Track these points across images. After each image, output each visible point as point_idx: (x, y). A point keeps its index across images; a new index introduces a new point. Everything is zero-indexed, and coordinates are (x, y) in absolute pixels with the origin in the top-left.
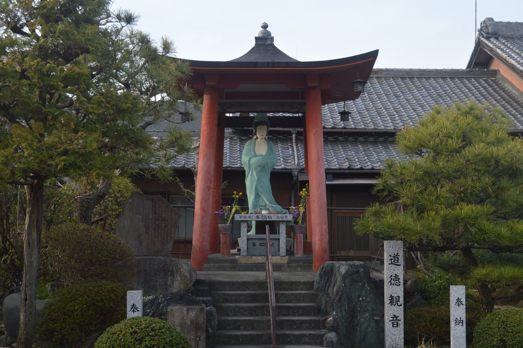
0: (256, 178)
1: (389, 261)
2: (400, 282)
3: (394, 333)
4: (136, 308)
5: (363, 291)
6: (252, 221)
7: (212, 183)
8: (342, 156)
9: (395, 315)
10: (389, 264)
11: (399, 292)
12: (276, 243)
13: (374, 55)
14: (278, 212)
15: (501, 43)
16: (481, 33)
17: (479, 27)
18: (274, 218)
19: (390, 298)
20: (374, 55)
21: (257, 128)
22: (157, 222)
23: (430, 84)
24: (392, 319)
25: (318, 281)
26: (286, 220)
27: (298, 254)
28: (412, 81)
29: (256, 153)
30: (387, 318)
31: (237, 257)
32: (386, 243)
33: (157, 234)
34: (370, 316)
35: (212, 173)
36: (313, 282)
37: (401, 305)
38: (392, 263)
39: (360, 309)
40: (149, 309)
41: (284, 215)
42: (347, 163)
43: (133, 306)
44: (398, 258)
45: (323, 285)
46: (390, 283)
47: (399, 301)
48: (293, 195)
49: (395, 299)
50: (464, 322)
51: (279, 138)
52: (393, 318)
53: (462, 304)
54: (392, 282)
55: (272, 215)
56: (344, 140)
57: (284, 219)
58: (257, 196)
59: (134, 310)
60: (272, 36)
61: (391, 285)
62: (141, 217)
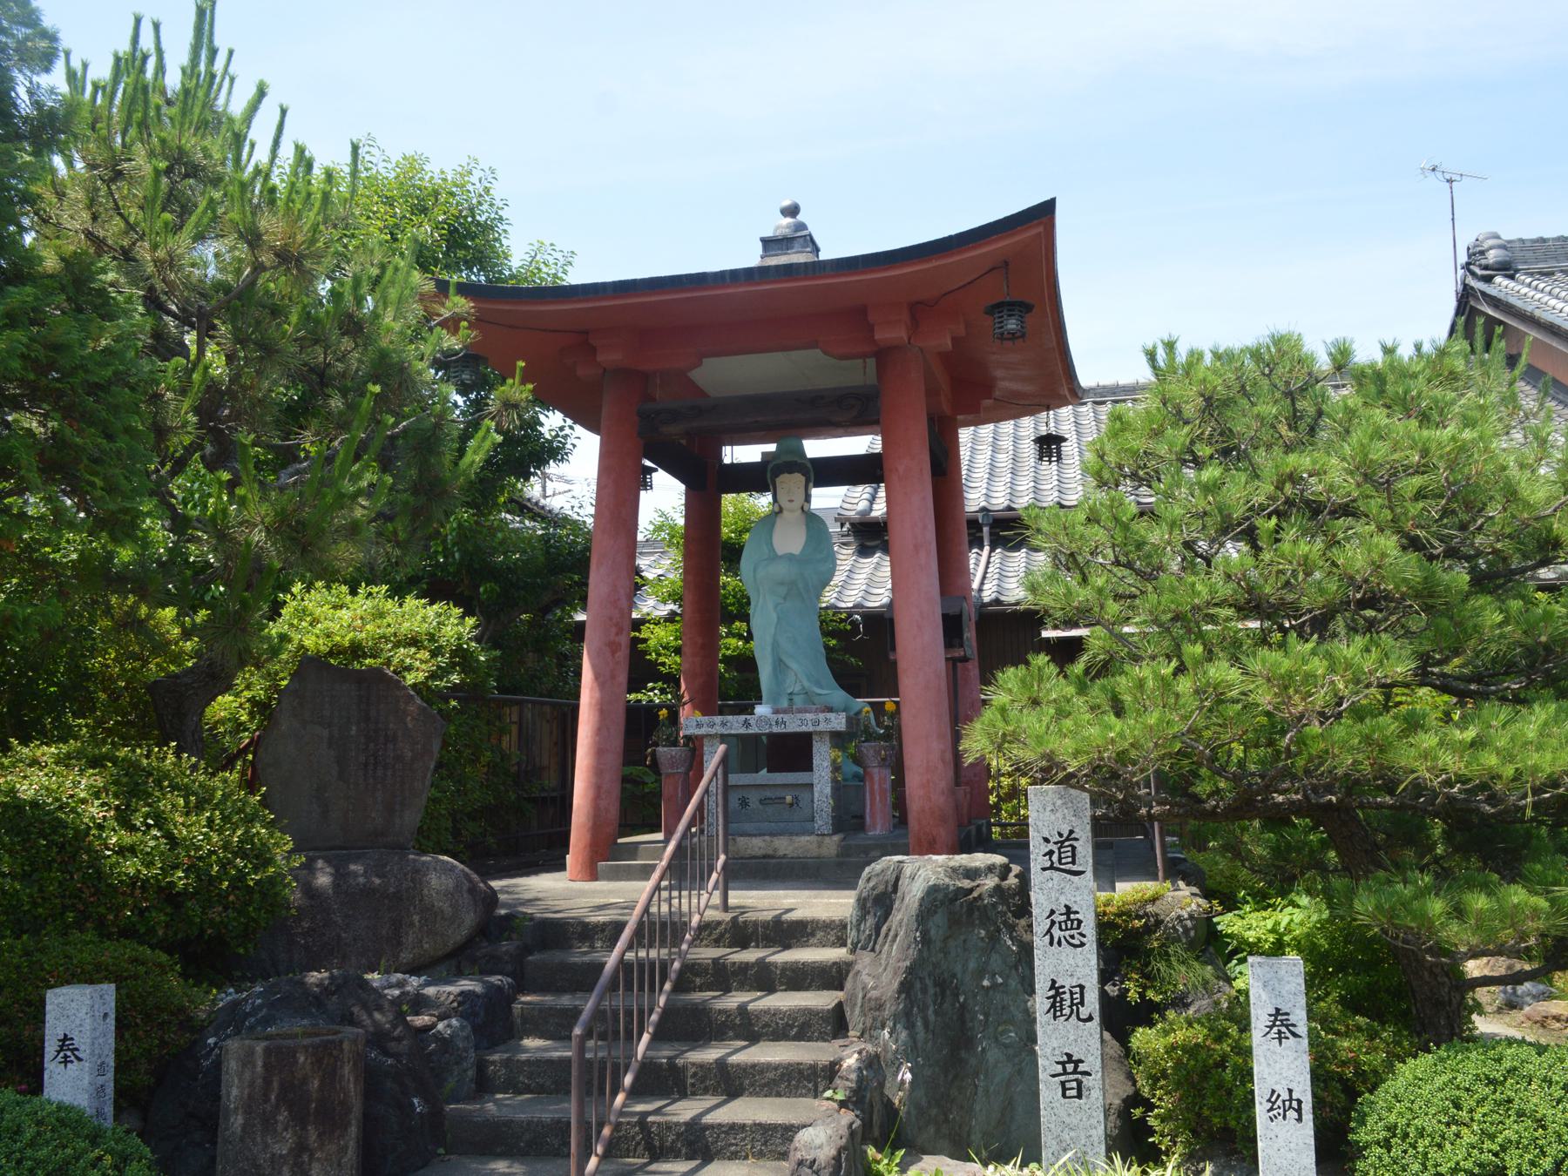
0: (774, 616)
2: (1084, 936)
3: (1068, 1120)
9: (1069, 1056)
10: (1044, 869)
11: (1080, 972)
12: (804, 796)
13: (1045, 211)
16: (1469, 271)
17: (1463, 258)
19: (1052, 993)
21: (778, 480)
24: (1059, 1068)
25: (854, 921)
26: (829, 727)
29: (775, 546)
30: (1047, 1064)
33: (371, 781)
34: (1021, 1039)
37: (1090, 1019)
38: (1052, 867)
39: (986, 1015)
40: (214, 1036)
44: (1074, 848)
46: (1048, 937)
47: (1082, 1003)
49: (1067, 996)
50: (1307, 1107)
52: (1063, 1064)
53: (1295, 1035)
54: (1056, 932)
55: (786, 717)
57: (822, 727)
58: (780, 666)
59: (66, 1057)
61: (1051, 944)
62: (326, 733)
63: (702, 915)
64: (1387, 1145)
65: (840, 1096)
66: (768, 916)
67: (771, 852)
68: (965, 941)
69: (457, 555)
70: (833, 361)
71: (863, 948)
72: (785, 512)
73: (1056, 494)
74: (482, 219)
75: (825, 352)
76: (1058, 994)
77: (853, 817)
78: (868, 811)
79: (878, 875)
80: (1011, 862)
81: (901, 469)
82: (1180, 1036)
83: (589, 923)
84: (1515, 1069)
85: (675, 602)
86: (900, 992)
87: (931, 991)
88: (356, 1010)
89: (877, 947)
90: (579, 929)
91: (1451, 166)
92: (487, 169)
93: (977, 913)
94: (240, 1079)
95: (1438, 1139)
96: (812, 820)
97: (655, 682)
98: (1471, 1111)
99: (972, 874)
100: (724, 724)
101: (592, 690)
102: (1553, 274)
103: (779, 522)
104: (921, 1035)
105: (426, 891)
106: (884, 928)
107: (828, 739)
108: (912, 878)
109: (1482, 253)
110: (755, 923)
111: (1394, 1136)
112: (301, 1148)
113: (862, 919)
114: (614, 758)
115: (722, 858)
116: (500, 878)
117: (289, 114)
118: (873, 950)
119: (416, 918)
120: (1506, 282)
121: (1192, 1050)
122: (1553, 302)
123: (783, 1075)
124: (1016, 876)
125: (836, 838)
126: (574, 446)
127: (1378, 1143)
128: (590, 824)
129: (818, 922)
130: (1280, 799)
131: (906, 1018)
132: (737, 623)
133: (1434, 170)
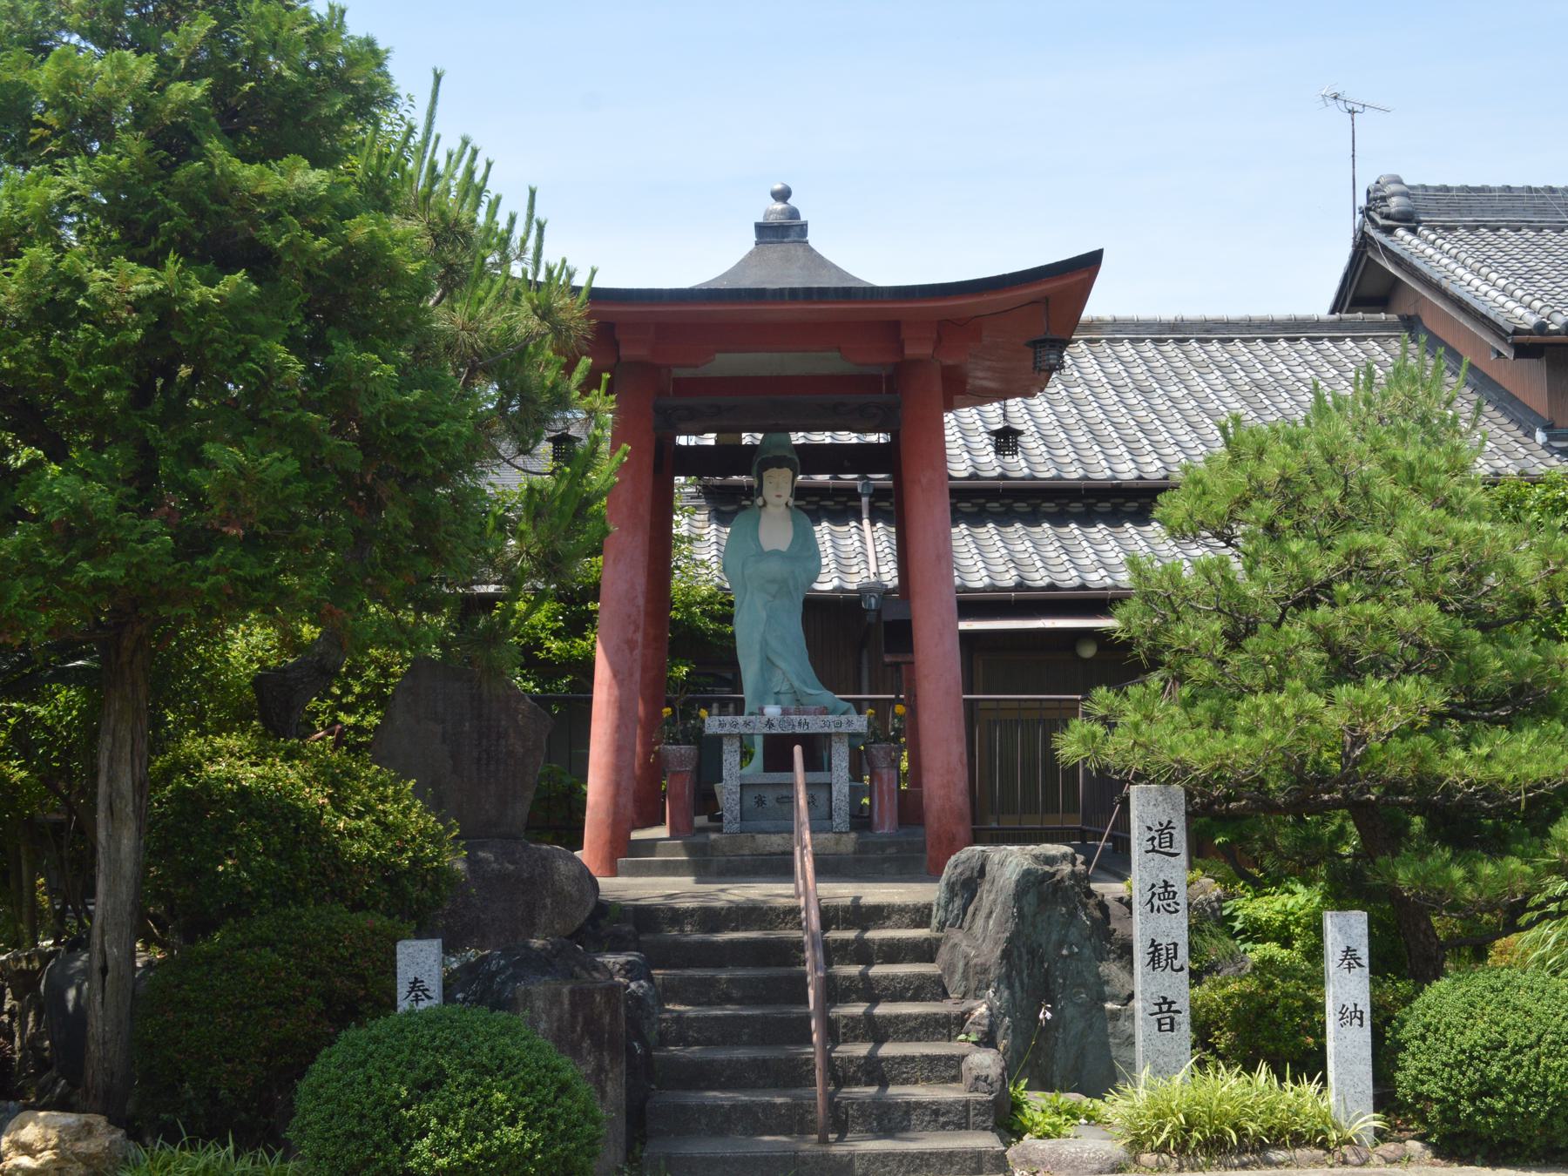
0: (764, 615)
1: (1144, 843)
3: (1162, 1048)
4: (423, 991)
5: (1073, 930)
6: (752, 734)
7: (641, 630)
8: (998, 555)
9: (1164, 999)
13: (1090, 263)
14: (826, 708)
15: (1426, 240)
17: (1362, 201)
18: (815, 724)
19: (1152, 949)
20: (1090, 263)
21: (765, 474)
22: (484, 742)
23: (1233, 357)
24: (1156, 1009)
25: (942, 903)
27: (883, 828)
28: (1185, 348)
31: (713, 836)
32: (1135, 791)
35: (641, 601)
36: (928, 907)
37: (1182, 969)
38: (1153, 850)
41: (843, 718)
42: (1013, 572)
43: (415, 984)
44: (1171, 835)
45: (958, 915)
47: (1175, 957)
48: (865, 661)
49: (1163, 952)
51: (825, 508)
52: (1159, 1005)
54: (1156, 902)
55: (809, 718)
57: (844, 729)
58: (768, 663)
59: (417, 996)
60: (803, 219)
61: (1152, 911)
64: (1423, 1038)
65: (973, 1038)
66: (848, 902)
68: (1049, 917)
71: (952, 926)
72: (769, 506)
76: (1156, 950)
81: (924, 481)
82: (1234, 987)
83: (678, 909)
84: (1509, 982)
86: (1002, 958)
87: (1025, 958)
88: (577, 969)
89: (966, 925)
90: (670, 914)
91: (1353, 94)
94: (548, 1016)
95: (1461, 1029)
96: (830, 817)
98: (1482, 1009)
99: (1050, 860)
102: (1455, 229)
104: (1019, 994)
105: (556, 877)
106: (971, 909)
108: (1002, 864)
109: (1384, 199)
111: (1428, 1030)
112: (600, 1069)
113: (950, 901)
117: (441, 140)
118: (960, 927)
119: (548, 901)
120: (1409, 237)
121: (1246, 997)
122: (1460, 271)
123: (922, 1023)
124: (1082, 863)
127: (1416, 1038)
130: (1326, 797)
131: (1007, 980)
133: (1336, 98)
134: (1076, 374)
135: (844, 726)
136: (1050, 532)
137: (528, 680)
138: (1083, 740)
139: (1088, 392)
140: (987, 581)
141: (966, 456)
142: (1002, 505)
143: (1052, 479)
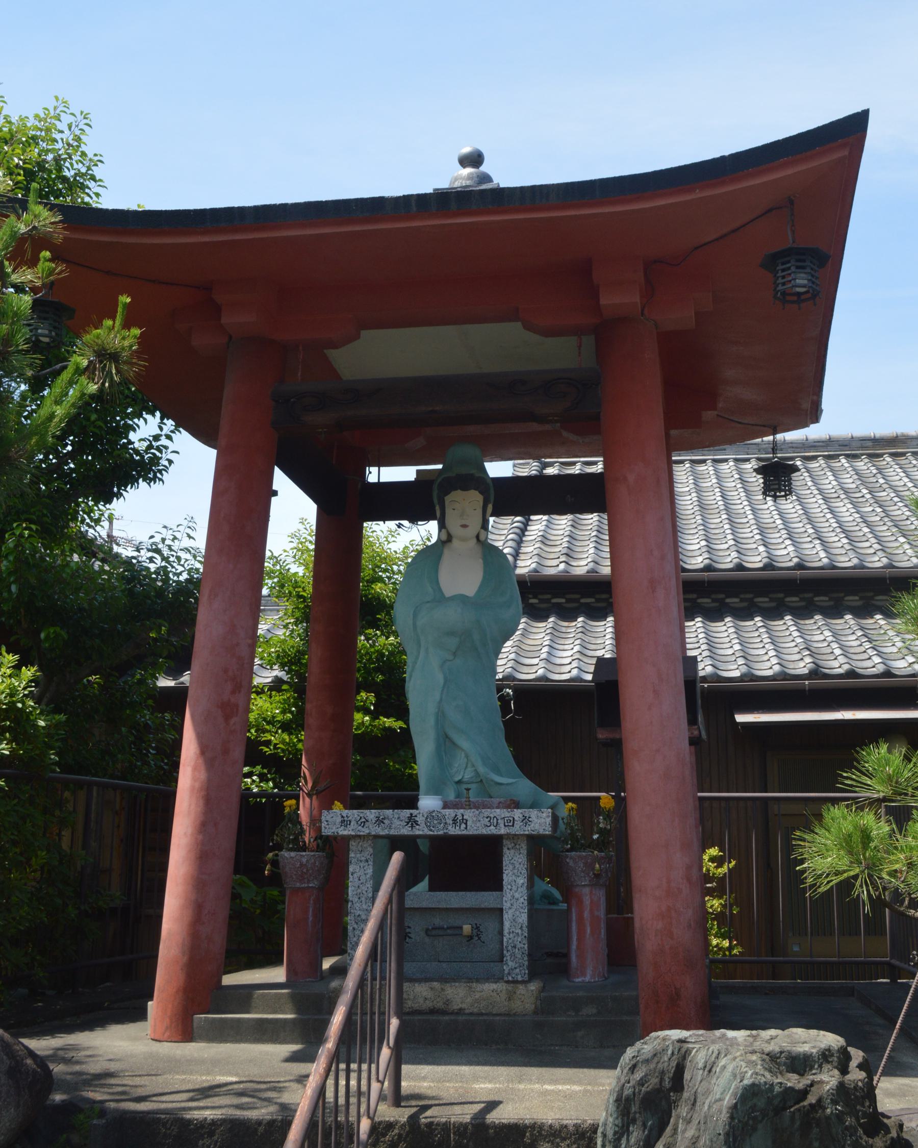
0: (440, 678)
12: (489, 926)
21: (448, 499)
26: (528, 830)
27: (584, 974)
36: (594, 1129)
42: (808, 660)
55: (469, 814)
56: (803, 604)
57: (518, 829)
63: (372, 1119)
66: (464, 1115)
67: (440, 1005)
69: (14, 588)
70: (534, 338)
73: (734, 554)
74: (68, 174)
75: (528, 327)
77: (549, 955)
78: (574, 946)
79: (647, 1061)
80: (848, 1045)
81: (631, 478)
83: (190, 1121)
85: (282, 666)
92: (78, 114)
93: (816, 1130)
96: (501, 959)
97: (253, 765)
100: (379, 821)
101: (195, 769)
103: (447, 553)
107: (524, 847)
108: (709, 1069)
110: (446, 1127)
113: (622, 1131)
114: (222, 867)
115: (394, 1023)
116: (52, 1031)
124: (860, 1067)
125: (533, 986)
126: (170, 462)
128: (185, 959)
129: (541, 1127)
132: (363, 694)
134: (881, 481)
135: (518, 824)
136: (852, 622)
137: (267, 781)
138: (847, 843)
139: (893, 495)
140: (777, 668)
141: (762, 549)
142: (802, 600)
143: (854, 567)
